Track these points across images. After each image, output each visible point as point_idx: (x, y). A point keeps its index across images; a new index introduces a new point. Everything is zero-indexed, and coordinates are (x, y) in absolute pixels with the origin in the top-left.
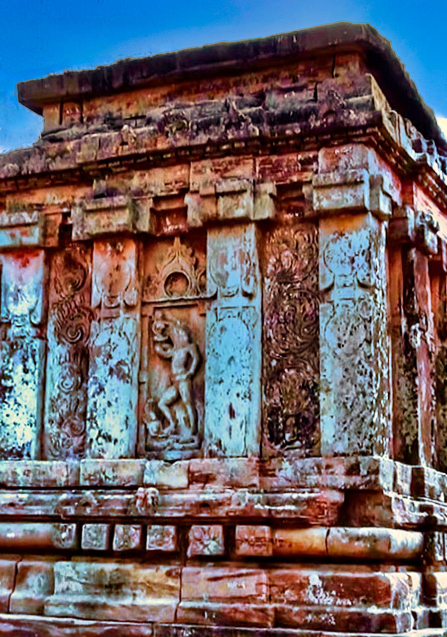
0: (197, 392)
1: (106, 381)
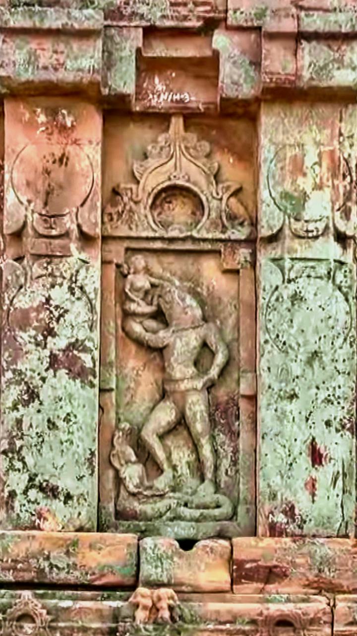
0: (231, 413)
1: (44, 380)
